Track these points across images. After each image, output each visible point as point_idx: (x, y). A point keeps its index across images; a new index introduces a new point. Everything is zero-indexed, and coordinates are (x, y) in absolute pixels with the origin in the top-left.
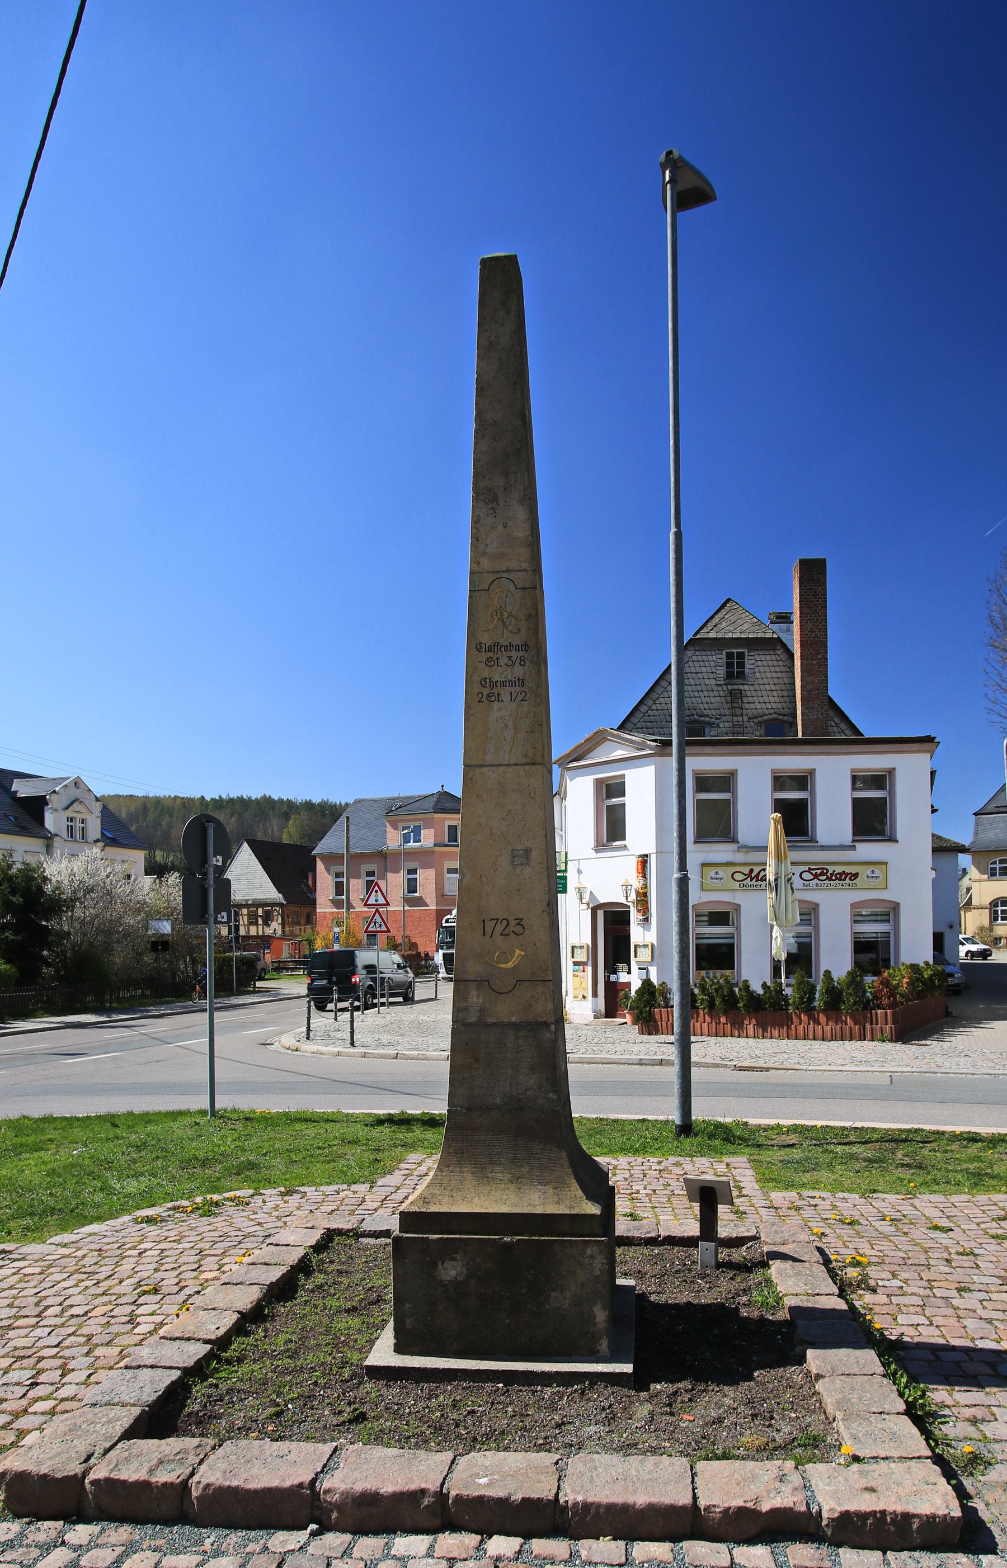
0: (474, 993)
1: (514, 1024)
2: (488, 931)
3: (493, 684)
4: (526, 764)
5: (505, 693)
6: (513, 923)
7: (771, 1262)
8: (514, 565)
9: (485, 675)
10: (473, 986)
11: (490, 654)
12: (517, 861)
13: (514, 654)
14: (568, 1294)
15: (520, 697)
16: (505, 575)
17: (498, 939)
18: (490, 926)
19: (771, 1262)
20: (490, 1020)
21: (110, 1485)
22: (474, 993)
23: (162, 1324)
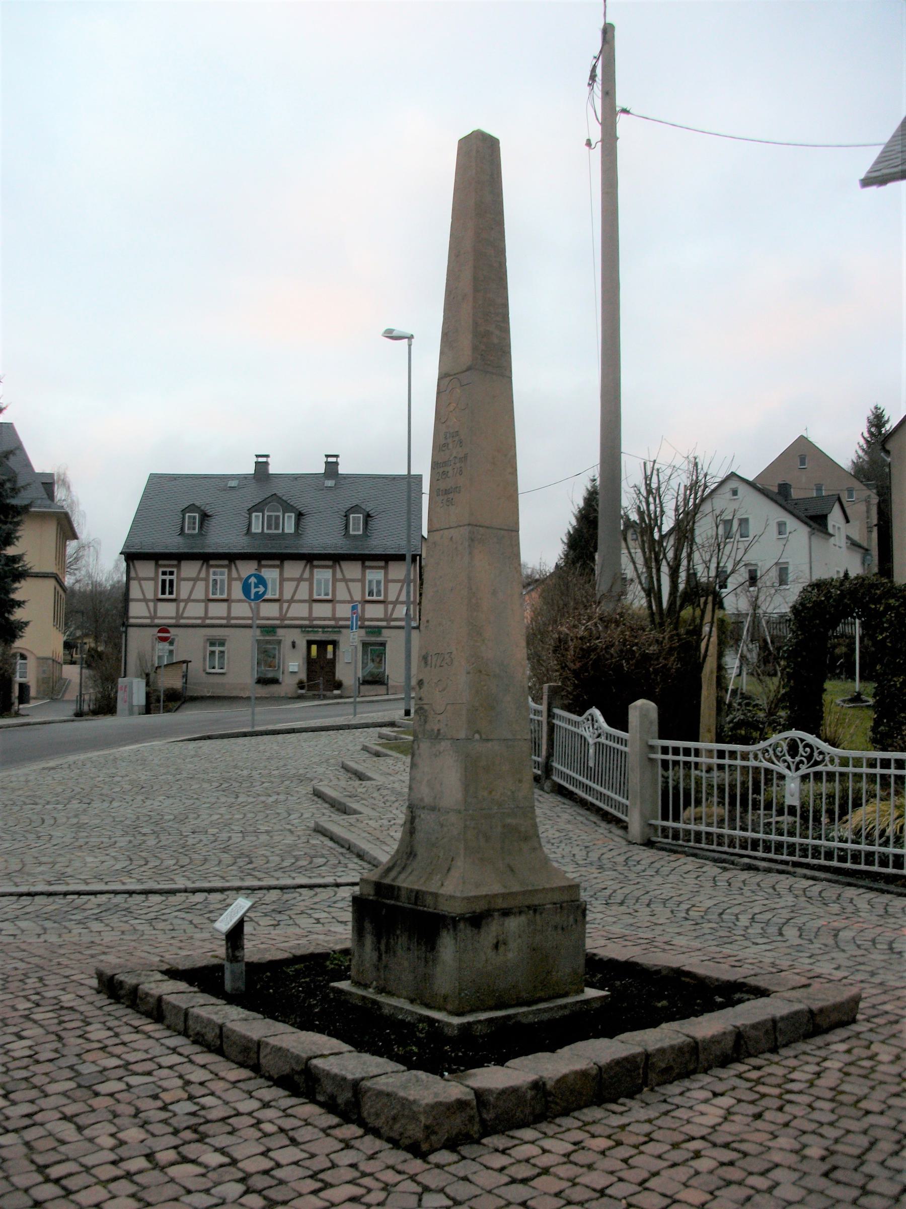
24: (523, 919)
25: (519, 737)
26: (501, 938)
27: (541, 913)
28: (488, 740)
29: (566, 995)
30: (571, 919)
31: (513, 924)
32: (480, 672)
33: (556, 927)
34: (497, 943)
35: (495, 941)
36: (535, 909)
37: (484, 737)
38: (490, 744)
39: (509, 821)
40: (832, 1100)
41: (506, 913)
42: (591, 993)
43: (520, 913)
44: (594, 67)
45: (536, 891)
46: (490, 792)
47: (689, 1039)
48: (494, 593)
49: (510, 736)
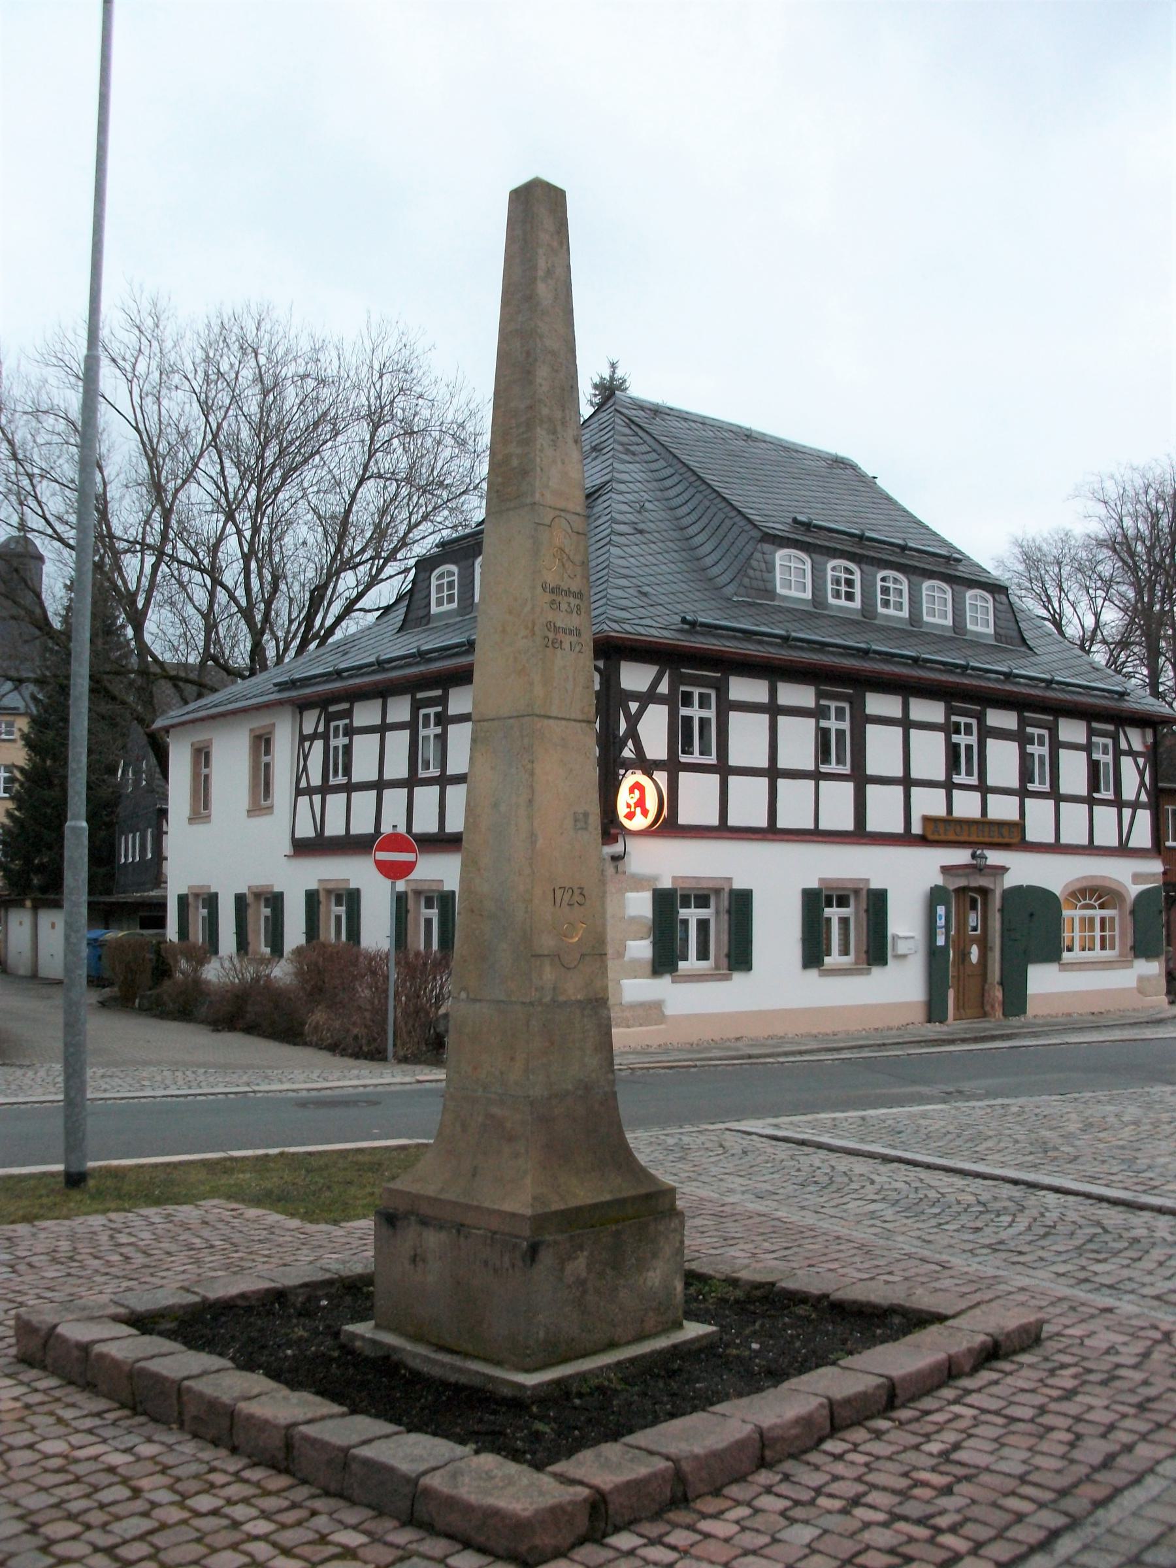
0: (548, 969)
1: (579, 1001)
2: (558, 901)
3: (557, 630)
4: (583, 721)
5: (567, 640)
6: (577, 892)
7: (685, 1323)
8: (571, 506)
9: (550, 619)
10: (547, 961)
11: (554, 597)
12: (579, 825)
13: (571, 600)
14: (658, 1271)
15: (577, 649)
16: (563, 514)
17: (566, 909)
18: (559, 893)
19: (685, 1323)
20: (562, 998)
21: (213, 1406)
22: (548, 969)
23: (320, 1257)
24: (443, 1236)
25: (514, 999)
26: (419, 1251)
27: (466, 1237)
28: (475, 1000)
29: (499, 1363)
30: (506, 1259)
31: (433, 1239)
32: (472, 911)
33: (486, 1263)
34: (415, 1255)
35: (412, 1253)
36: (460, 1228)
37: (472, 996)
38: (478, 1005)
39: (495, 1110)
40: (1063, 1457)
41: (424, 1222)
42: (693, 1330)
43: (441, 1228)
44: (1090, 1306)
45: (229, 1197)
46: (475, 1068)
47: (881, 1380)
48: (495, 805)
49: (502, 997)
